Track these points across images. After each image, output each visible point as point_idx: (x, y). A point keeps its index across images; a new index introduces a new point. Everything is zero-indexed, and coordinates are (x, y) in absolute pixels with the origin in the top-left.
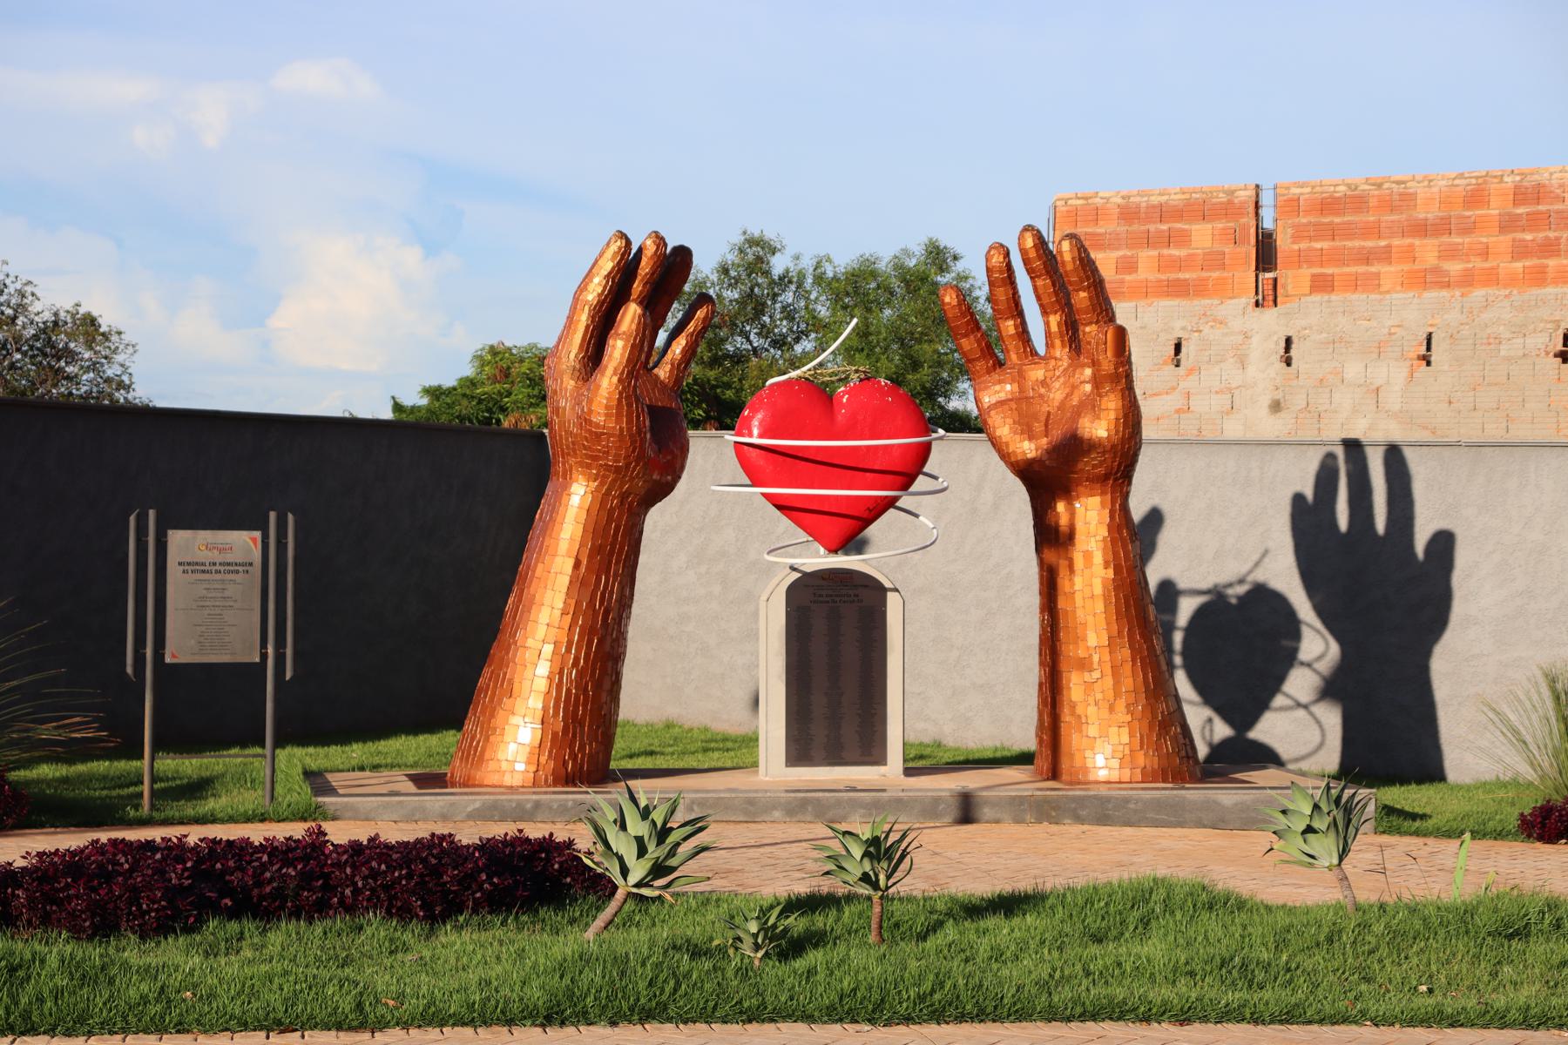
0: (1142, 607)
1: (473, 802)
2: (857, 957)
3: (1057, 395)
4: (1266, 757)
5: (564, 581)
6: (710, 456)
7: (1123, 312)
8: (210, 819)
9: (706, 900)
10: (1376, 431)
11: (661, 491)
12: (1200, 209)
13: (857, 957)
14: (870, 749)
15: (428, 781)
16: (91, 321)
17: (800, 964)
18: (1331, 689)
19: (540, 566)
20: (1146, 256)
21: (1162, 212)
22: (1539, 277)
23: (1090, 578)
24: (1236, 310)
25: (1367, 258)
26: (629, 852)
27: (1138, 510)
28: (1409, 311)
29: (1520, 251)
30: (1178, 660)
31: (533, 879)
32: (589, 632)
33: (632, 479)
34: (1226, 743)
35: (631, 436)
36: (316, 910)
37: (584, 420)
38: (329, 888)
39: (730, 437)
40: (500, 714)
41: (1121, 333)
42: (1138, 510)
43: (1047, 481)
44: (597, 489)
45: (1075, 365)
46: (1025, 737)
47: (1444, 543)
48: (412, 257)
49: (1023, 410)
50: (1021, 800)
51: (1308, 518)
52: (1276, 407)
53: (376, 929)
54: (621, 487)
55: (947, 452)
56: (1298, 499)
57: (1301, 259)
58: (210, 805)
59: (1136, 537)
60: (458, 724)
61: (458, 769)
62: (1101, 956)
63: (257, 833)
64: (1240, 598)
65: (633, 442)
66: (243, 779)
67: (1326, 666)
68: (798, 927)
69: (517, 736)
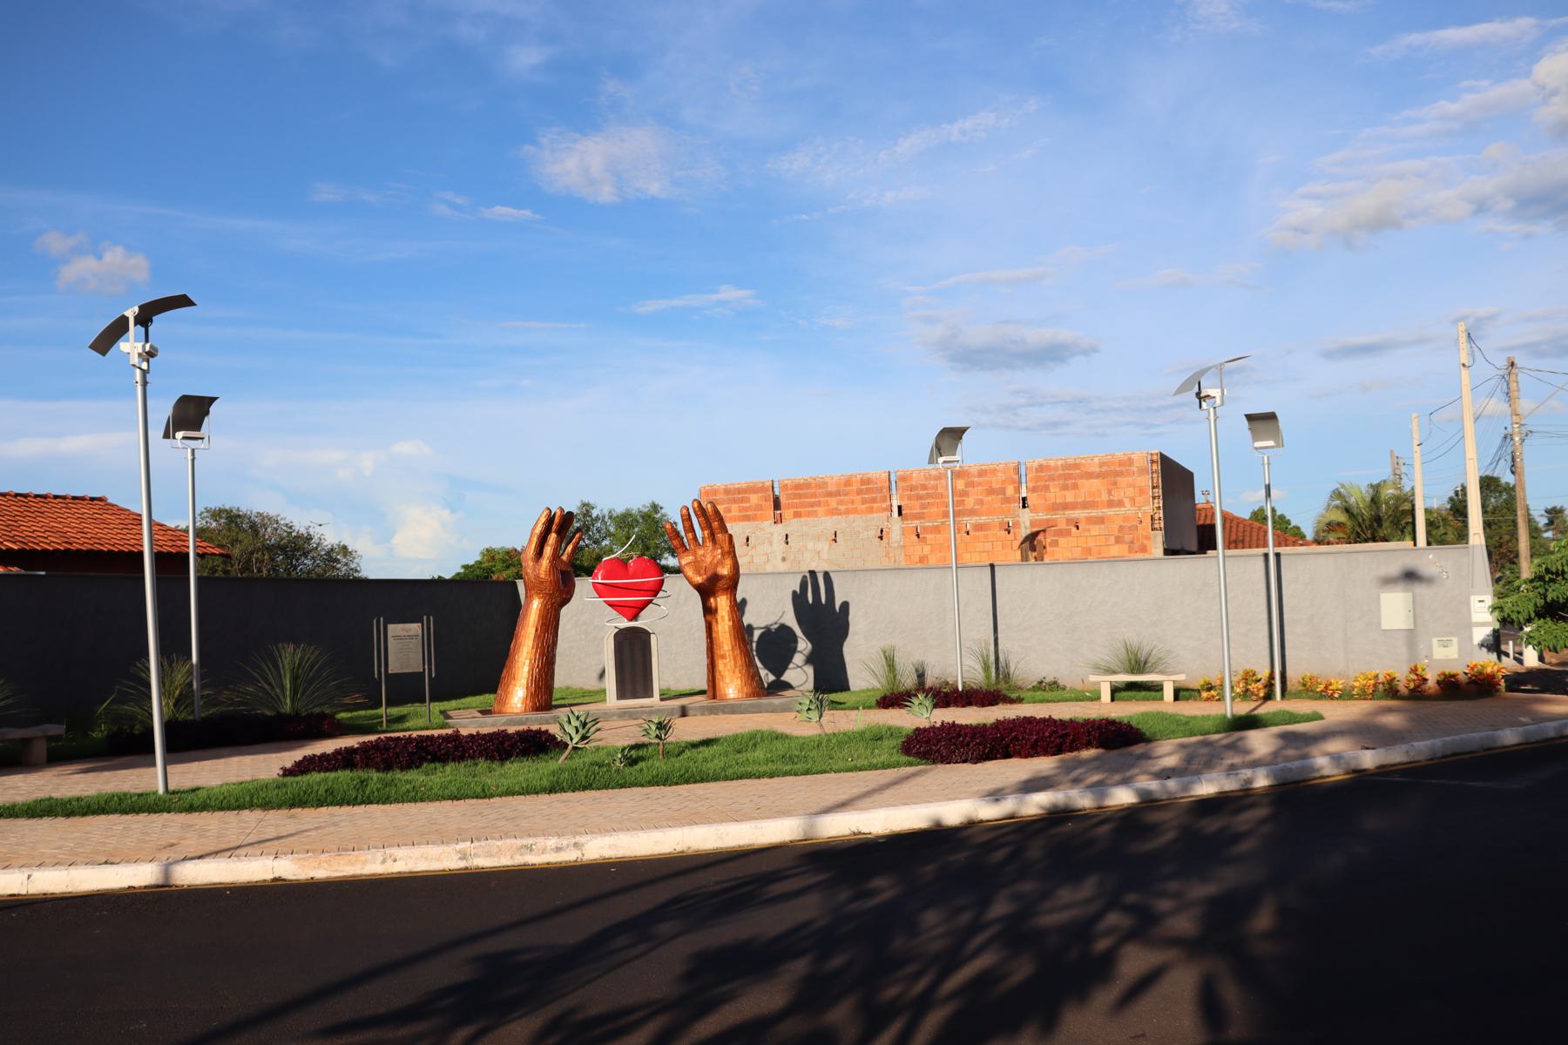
0: (742, 632)
1: (503, 719)
3: (708, 559)
4: (788, 686)
5: (532, 636)
6: (583, 586)
7: (732, 528)
8: (408, 730)
9: (598, 749)
10: (820, 568)
11: (566, 601)
13: (657, 764)
14: (648, 693)
15: (485, 712)
16: (345, 548)
20: (734, 507)
21: (739, 491)
22: (871, 510)
23: (724, 625)
25: (812, 505)
28: (828, 524)
29: (864, 501)
31: (536, 744)
32: (542, 654)
36: (461, 758)
37: (537, 577)
38: (465, 751)
39: (590, 580)
43: (706, 591)
45: (714, 548)
46: (703, 684)
47: (845, 605)
48: (446, 513)
49: (696, 565)
50: (702, 708)
51: (798, 599)
52: (784, 559)
53: (483, 764)
55: (670, 581)
56: (794, 593)
57: (790, 506)
58: (407, 725)
59: (739, 608)
60: (494, 691)
61: (496, 708)
62: (741, 757)
63: (436, 733)
64: (60, 723)
66: (416, 714)
67: (806, 652)
68: (634, 755)
69: (518, 695)
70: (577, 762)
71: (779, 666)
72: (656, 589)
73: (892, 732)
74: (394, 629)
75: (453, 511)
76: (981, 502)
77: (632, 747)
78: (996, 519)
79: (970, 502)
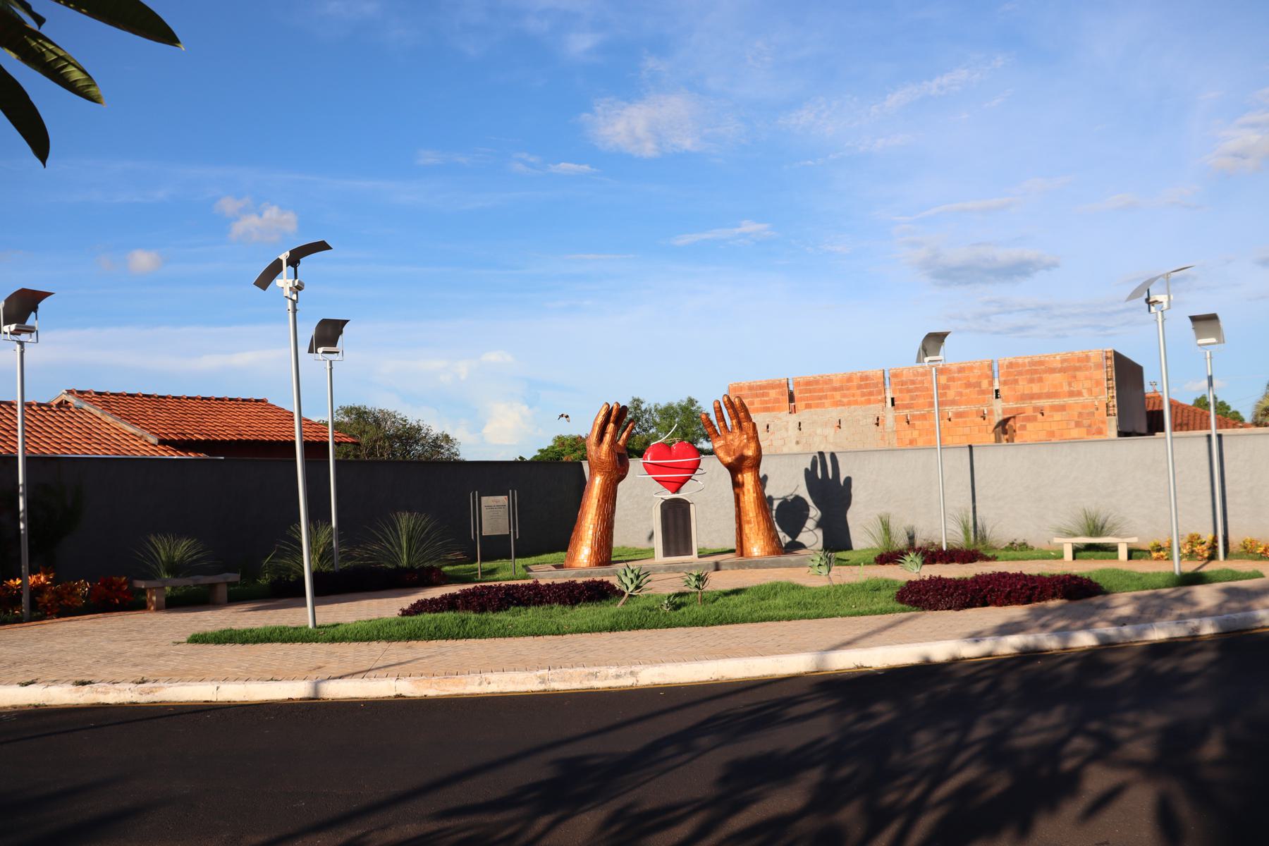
0: (764, 502)
1: (573, 572)
2: (696, 609)
3: (736, 443)
4: (801, 546)
6: (636, 465)
7: (755, 417)
9: (648, 596)
10: (827, 449)
11: (622, 478)
12: (772, 386)
14: (688, 551)
15: (558, 567)
16: (447, 436)
17: (681, 611)
18: (819, 525)
20: (757, 400)
21: (761, 387)
22: (869, 402)
23: (749, 497)
24: (784, 414)
26: (629, 583)
27: (761, 475)
28: (834, 413)
29: (863, 395)
31: (599, 592)
32: (603, 521)
36: (540, 603)
39: (641, 461)
41: (754, 425)
42: (761, 475)
43: (735, 469)
47: (848, 480)
48: (525, 408)
49: (727, 448)
51: (810, 475)
52: (797, 443)
53: (557, 608)
56: (806, 470)
57: (801, 399)
58: (497, 576)
59: (761, 482)
60: (566, 550)
61: (567, 563)
62: (765, 604)
66: (504, 568)
67: (817, 518)
68: (678, 602)
69: (584, 552)
70: (632, 607)
71: (794, 530)
72: (694, 468)
73: (888, 584)
74: (487, 501)
75: (531, 406)
76: (960, 394)
77: (677, 595)
78: (973, 408)
79: (951, 394)
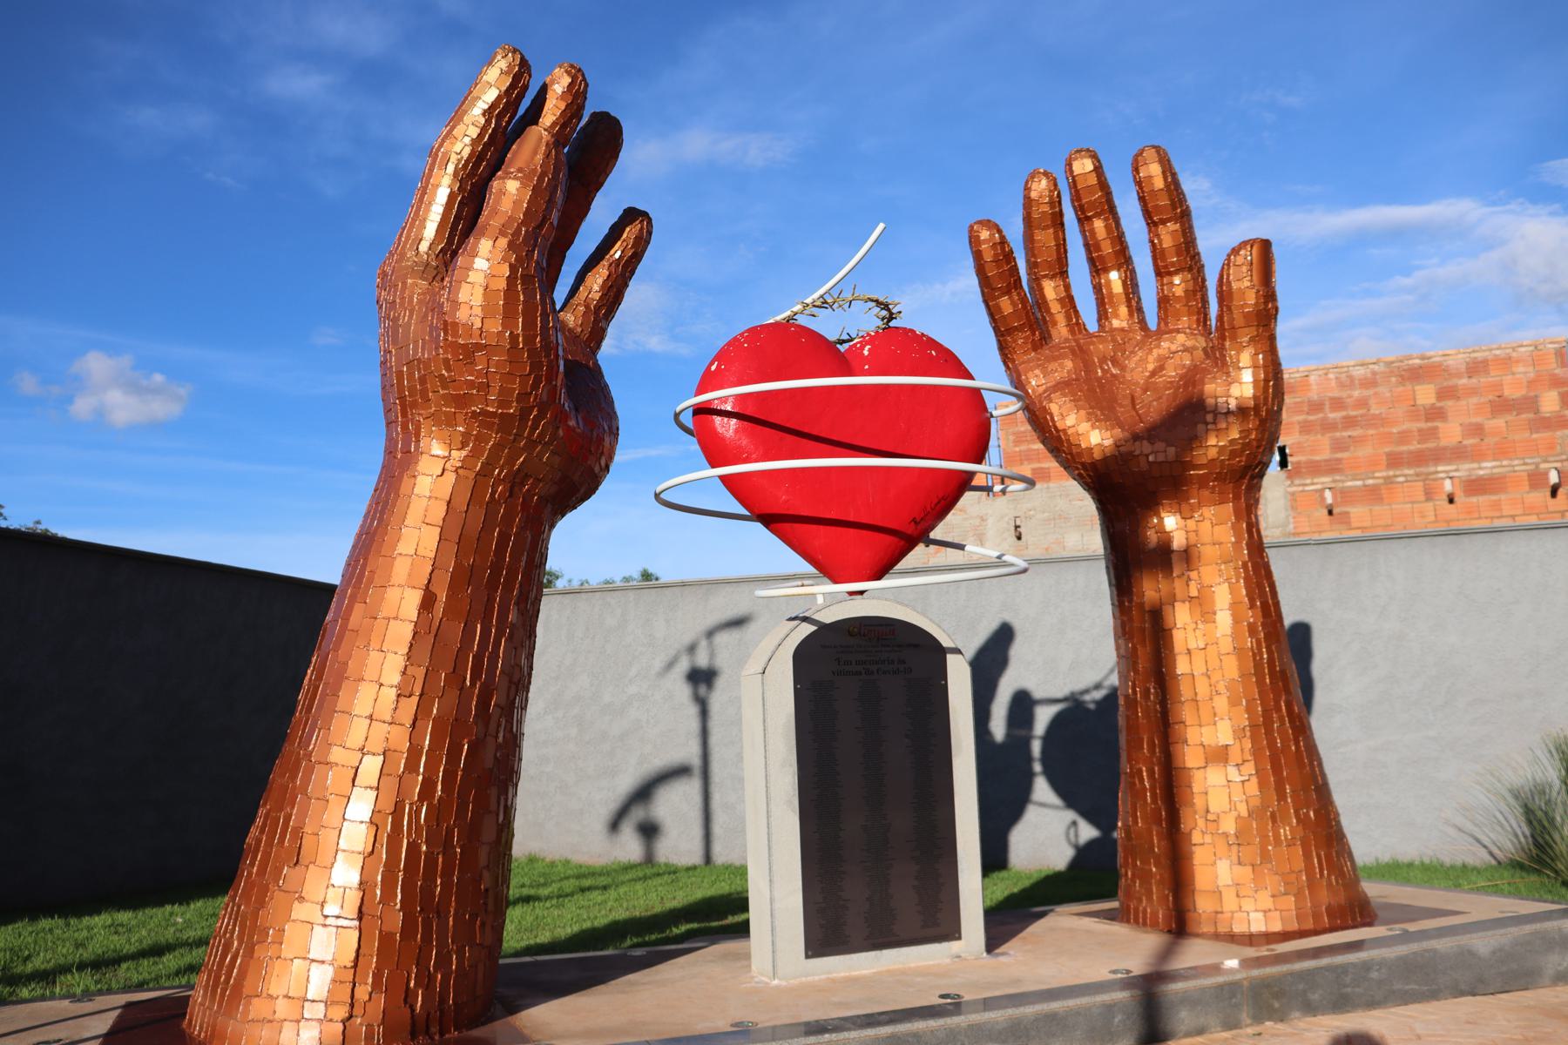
5: (402, 633)
19: (358, 609)
30: (1037, 767)
32: (450, 730)
33: (532, 444)
34: (1091, 844)
35: (532, 353)
40: (276, 898)
43: (1125, 493)
44: (465, 464)
54: (511, 460)
64: (1098, 703)
65: (536, 366)
76: (1477, 430)
78: (1519, 466)
79: (1451, 432)
